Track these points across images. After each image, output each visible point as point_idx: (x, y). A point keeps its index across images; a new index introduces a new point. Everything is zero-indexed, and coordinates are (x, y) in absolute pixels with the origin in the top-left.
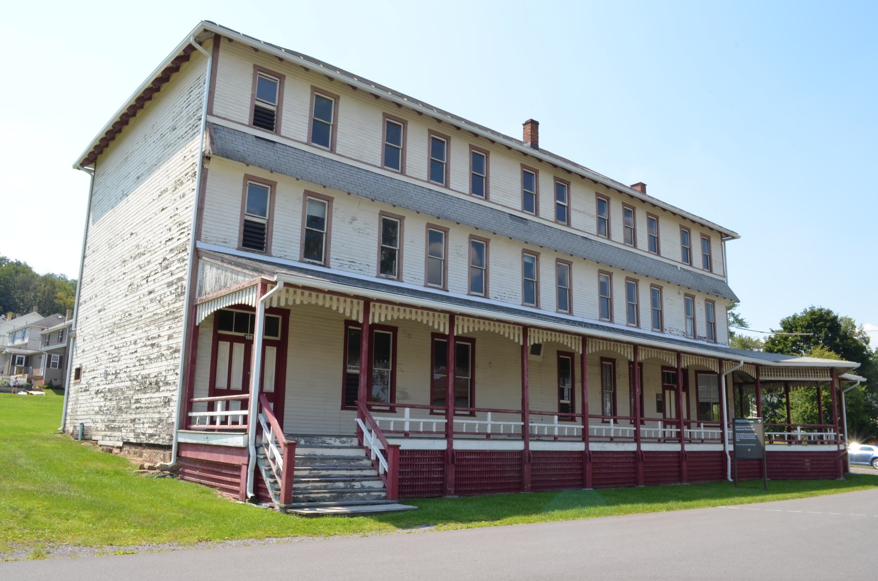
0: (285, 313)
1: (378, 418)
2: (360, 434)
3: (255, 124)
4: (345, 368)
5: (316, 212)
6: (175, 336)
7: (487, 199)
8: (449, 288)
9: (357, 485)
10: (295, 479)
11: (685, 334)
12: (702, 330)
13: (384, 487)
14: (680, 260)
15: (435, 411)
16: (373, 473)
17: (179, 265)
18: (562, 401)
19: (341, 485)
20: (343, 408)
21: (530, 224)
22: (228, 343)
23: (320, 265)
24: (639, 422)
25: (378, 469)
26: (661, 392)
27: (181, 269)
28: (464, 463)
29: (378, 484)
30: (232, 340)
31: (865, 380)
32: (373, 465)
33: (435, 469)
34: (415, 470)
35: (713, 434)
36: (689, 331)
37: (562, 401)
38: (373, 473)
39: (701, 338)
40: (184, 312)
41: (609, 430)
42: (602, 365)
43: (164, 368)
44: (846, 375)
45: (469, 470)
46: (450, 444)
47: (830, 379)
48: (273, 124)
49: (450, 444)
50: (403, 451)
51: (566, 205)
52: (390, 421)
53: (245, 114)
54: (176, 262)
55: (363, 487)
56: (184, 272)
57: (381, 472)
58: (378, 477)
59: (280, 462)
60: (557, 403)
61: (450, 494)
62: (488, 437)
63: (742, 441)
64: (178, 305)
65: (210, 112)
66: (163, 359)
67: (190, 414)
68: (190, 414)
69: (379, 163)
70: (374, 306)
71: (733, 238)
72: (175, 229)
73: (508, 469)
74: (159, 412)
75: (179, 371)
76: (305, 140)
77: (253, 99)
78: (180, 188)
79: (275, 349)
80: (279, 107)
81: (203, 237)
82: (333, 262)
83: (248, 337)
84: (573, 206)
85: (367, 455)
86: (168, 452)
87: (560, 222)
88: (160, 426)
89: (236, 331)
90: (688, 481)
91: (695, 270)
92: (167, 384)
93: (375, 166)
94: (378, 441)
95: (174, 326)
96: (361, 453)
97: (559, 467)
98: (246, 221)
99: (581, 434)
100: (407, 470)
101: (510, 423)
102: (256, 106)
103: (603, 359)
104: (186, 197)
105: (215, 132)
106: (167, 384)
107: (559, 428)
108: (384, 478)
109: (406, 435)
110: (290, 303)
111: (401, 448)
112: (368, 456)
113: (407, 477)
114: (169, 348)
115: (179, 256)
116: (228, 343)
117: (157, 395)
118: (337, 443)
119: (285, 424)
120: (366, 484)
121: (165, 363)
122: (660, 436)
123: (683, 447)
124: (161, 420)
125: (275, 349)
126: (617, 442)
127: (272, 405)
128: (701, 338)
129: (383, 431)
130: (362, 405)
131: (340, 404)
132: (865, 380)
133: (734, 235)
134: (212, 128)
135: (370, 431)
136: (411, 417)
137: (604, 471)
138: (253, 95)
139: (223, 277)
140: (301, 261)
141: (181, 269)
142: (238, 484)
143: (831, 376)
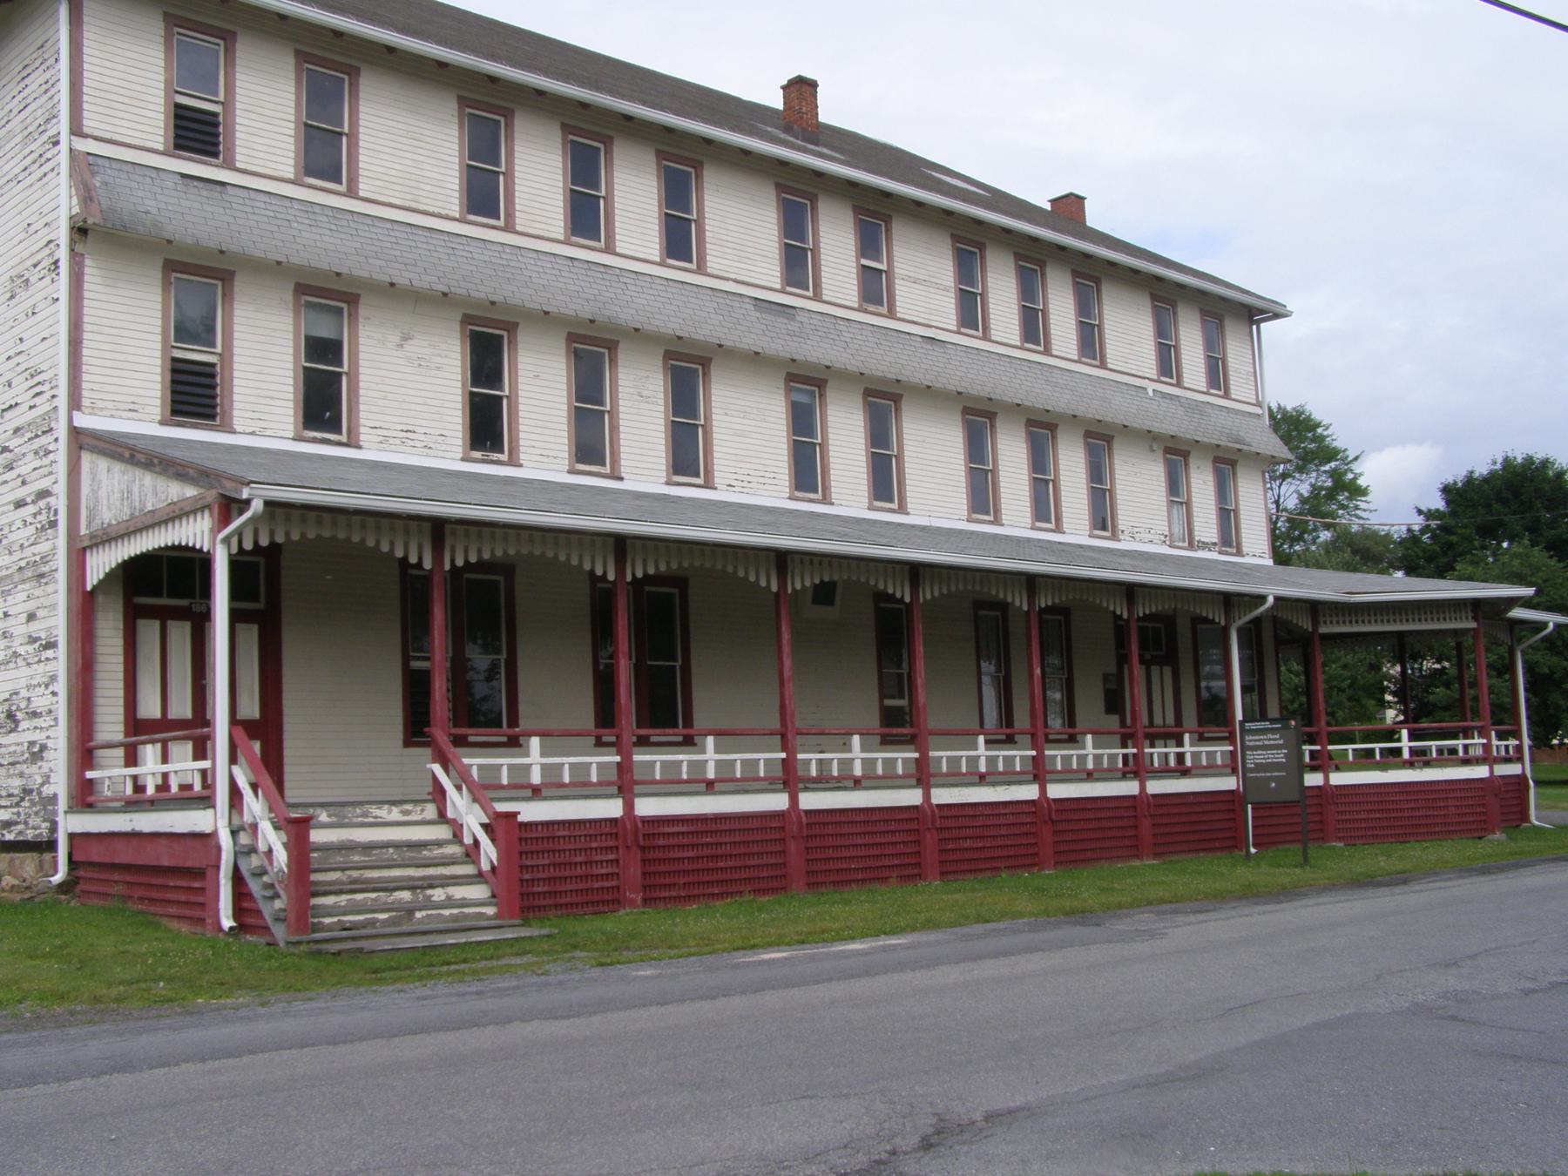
0: (273, 552)
1: (474, 762)
2: (439, 794)
3: (177, 146)
4: (406, 660)
5: (324, 331)
6: (40, 613)
7: (701, 269)
8: (624, 471)
9: (438, 894)
10: (313, 889)
11: (1170, 539)
12: (1207, 526)
13: (494, 896)
14: (1153, 373)
15: (605, 739)
16: (468, 869)
17: (37, 463)
18: (889, 702)
19: (406, 895)
20: (408, 743)
21: (801, 317)
22: (157, 624)
23: (339, 444)
24: (1041, 739)
25: (476, 862)
26: (1113, 669)
27: (44, 471)
28: (661, 842)
29: (479, 892)
30: (164, 615)
32: (468, 855)
33: (599, 858)
34: (558, 860)
35: (1211, 755)
36: (1177, 530)
37: (889, 702)
38: (468, 869)
39: (1205, 546)
40: (61, 562)
41: (973, 761)
42: (976, 618)
43: (23, 683)
44: (1518, 613)
45: (671, 855)
46: (629, 806)
47: (1473, 625)
48: (217, 144)
49: (629, 806)
50: (522, 825)
51: (883, 267)
52: (504, 763)
53: (153, 127)
54: (31, 456)
55: (449, 898)
56: (52, 478)
57: (485, 866)
58: (480, 877)
59: (281, 857)
60: (877, 704)
61: (633, 903)
62: (710, 787)
63: (1260, 767)
64: (43, 547)
65: (77, 130)
66: (20, 662)
67: (90, 775)
68: (90, 775)
69: (455, 210)
70: (454, 534)
71: (1276, 316)
72: (21, 385)
74: (21, 775)
75: (61, 686)
76: (289, 172)
77: (170, 91)
78: (24, 295)
79: (255, 628)
80: (228, 104)
81: (85, 402)
82: (365, 436)
83: (197, 608)
84: (900, 269)
85: (455, 835)
86: (47, 856)
87: (871, 308)
88: (26, 804)
89: (170, 595)
90: (1156, 855)
91: (1189, 394)
92: (35, 714)
93: (447, 218)
94: (476, 806)
95: (37, 592)
96: (442, 832)
97: (868, 840)
98: (174, 360)
99: (1228, 761)
100: (541, 862)
101: (681, 757)
102: (178, 106)
103: (979, 604)
104: (38, 317)
105: (93, 174)
106: (35, 714)
107: (544, 767)
108: (490, 877)
109: (536, 793)
110: (280, 539)
111: (520, 818)
112: (457, 837)
113: (541, 875)
114: (33, 640)
115: (37, 443)
116: (157, 624)
117: (13, 738)
118: (395, 814)
119: (287, 785)
120: (459, 892)
121: (25, 671)
122: (858, 771)
123: (1143, 788)
124: (27, 791)
125: (255, 628)
126: (994, 784)
127: (257, 746)
128: (1205, 546)
129: (486, 787)
130: (440, 733)
131: (401, 736)
133: (1278, 310)
134: (83, 167)
135: (459, 788)
136: (543, 755)
137: (968, 843)
138: (168, 83)
139: (136, 490)
140: (298, 438)
141: (44, 471)
142: (202, 905)
143: (1475, 618)
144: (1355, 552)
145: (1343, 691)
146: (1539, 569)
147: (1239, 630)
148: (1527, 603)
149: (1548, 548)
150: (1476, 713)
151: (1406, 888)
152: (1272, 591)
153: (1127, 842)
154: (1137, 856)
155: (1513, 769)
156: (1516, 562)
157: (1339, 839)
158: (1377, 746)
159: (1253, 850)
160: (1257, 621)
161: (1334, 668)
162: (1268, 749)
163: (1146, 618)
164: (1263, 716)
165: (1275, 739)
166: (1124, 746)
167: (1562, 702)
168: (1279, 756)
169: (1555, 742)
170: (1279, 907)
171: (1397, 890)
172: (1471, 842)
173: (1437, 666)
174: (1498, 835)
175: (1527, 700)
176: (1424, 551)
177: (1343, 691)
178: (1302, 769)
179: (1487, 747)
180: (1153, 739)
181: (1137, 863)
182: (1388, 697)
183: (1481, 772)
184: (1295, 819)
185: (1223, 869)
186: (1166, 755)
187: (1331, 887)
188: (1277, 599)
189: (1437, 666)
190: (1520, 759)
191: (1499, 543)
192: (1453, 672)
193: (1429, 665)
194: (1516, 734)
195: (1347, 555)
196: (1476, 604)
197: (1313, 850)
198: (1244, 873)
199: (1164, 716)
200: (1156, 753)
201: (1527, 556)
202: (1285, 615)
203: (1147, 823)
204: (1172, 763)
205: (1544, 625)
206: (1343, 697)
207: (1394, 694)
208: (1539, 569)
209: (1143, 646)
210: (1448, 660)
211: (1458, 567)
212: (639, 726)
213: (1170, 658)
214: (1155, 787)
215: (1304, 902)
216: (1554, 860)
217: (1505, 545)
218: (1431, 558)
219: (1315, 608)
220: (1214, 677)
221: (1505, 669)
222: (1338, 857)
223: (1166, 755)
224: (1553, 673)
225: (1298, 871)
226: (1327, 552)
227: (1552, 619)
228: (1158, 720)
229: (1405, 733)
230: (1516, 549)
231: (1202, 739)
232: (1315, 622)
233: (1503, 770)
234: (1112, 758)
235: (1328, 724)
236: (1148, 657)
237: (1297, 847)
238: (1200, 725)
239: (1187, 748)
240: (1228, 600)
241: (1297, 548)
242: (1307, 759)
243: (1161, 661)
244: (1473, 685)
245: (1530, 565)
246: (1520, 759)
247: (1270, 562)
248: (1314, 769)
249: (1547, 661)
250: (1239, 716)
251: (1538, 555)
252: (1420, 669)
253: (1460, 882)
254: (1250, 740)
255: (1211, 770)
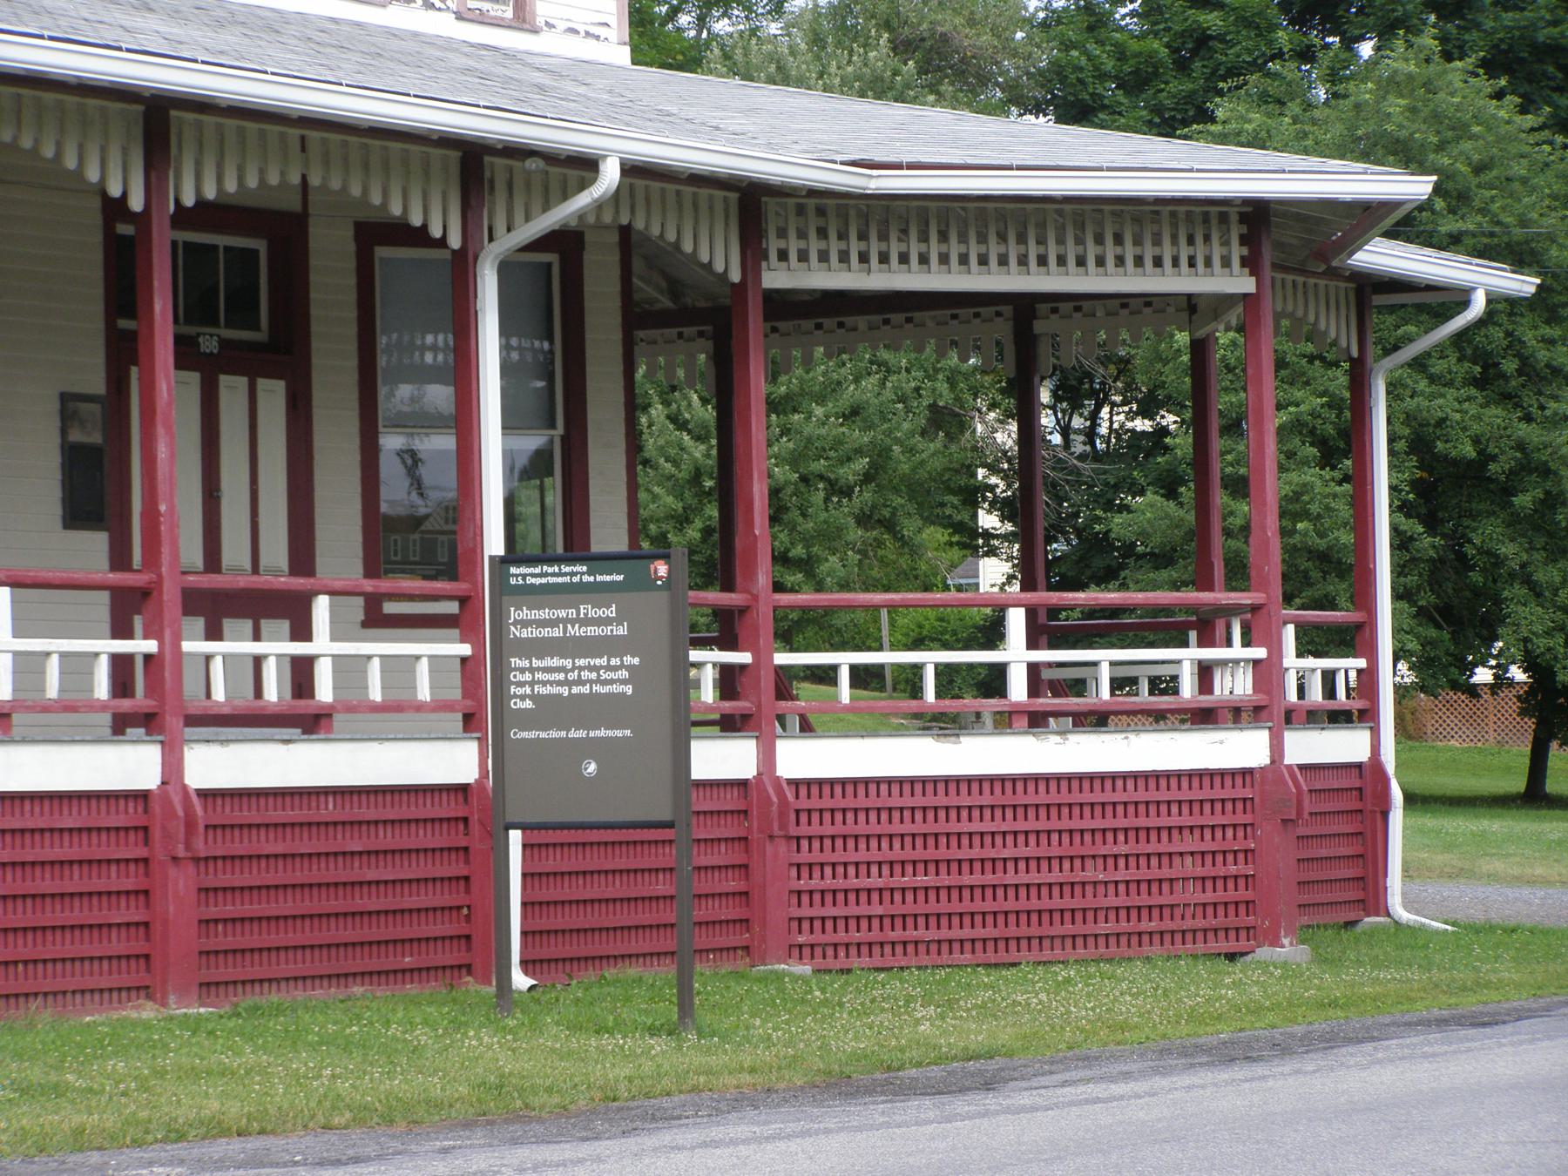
22: (244, 380)
26: (96, 383)
31: (1524, 284)
44: (1382, 255)
47: (1247, 285)
63: (550, 710)
73: (1093, 873)
90: (209, 988)
116: (244, 380)
123: (172, 767)
132: (1524, 284)
143: (1251, 264)
144: (902, 48)
145: (847, 492)
146: (1461, 130)
147: (506, 270)
148: (1407, 224)
149: (1491, 66)
150: (1238, 573)
151: (991, 1100)
152: (616, 145)
153: (117, 944)
154: (144, 990)
155: (1344, 746)
156: (1396, 105)
157: (799, 951)
158: (930, 659)
159: (521, 980)
160: (566, 242)
161: (818, 421)
162: (580, 649)
163: (206, 214)
164: (576, 546)
165: (603, 619)
166: (121, 630)
167: (1507, 549)
168: (613, 677)
169: (1483, 675)
170: (586, 1149)
171: (960, 1104)
172: (1202, 969)
173: (1142, 425)
174: (1288, 950)
175: (1401, 542)
176: (1121, 54)
177: (847, 492)
178: (685, 725)
179: (1267, 673)
180: (217, 608)
181: (148, 1012)
182: (988, 520)
183: (1244, 748)
184: (662, 887)
185: (422, 1036)
186: (258, 661)
187: (758, 1094)
188: (633, 170)
189: (1142, 425)
190: (1367, 716)
191: (1349, 43)
192: (1182, 444)
193: (1114, 419)
194: (1353, 639)
195: (880, 54)
196: (1255, 218)
197: (708, 980)
198: (488, 1049)
199: (257, 546)
200: (219, 659)
201: (1429, 86)
202: (653, 225)
203: (180, 884)
204: (273, 691)
205: (1459, 298)
206: (843, 513)
207: (1006, 509)
208: (1461, 130)
209: (196, 306)
210: (1177, 408)
211: (1222, 109)
212: (18, 633)
213: (283, 354)
214: (216, 765)
215: (666, 1137)
216: (1442, 1023)
217: (1366, 49)
218: (1138, 80)
219: (752, 205)
220: (427, 421)
221: (1342, 445)
222: (786, 1007)
223: (258, 661)
224: (1485, 458)
225: (658, 1045)
226: (817, 40)
227: (1486, 281)
228: (235, 551)
229: (1016, 621)
230: (1401, 62)
231: (376, 620)
232: (753, 252)
233: (1313, 747)
234: (76, 665)
235: (778, 587)
236: (209, 345)
237: (664, 974)
238: (371, 571)
239: (322, 644)
240: (475, 166)
241: (722, 26)
242: (708, 693)
243: (251, 362)
244: (1239, 487)
245: (1436, 117)
246: (1367, 716)
247: (623, 55)
248: (730, 725)
249: (1470, 422)
250: (494, 543)
251: (1463, 87)
252: (1091, 434)
253: (1159, 1082)
254: (524, 621)
255: (396, 715)
